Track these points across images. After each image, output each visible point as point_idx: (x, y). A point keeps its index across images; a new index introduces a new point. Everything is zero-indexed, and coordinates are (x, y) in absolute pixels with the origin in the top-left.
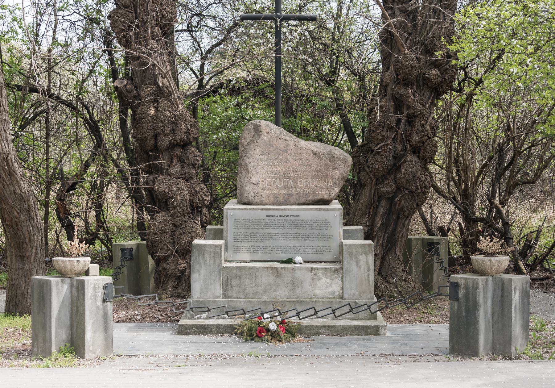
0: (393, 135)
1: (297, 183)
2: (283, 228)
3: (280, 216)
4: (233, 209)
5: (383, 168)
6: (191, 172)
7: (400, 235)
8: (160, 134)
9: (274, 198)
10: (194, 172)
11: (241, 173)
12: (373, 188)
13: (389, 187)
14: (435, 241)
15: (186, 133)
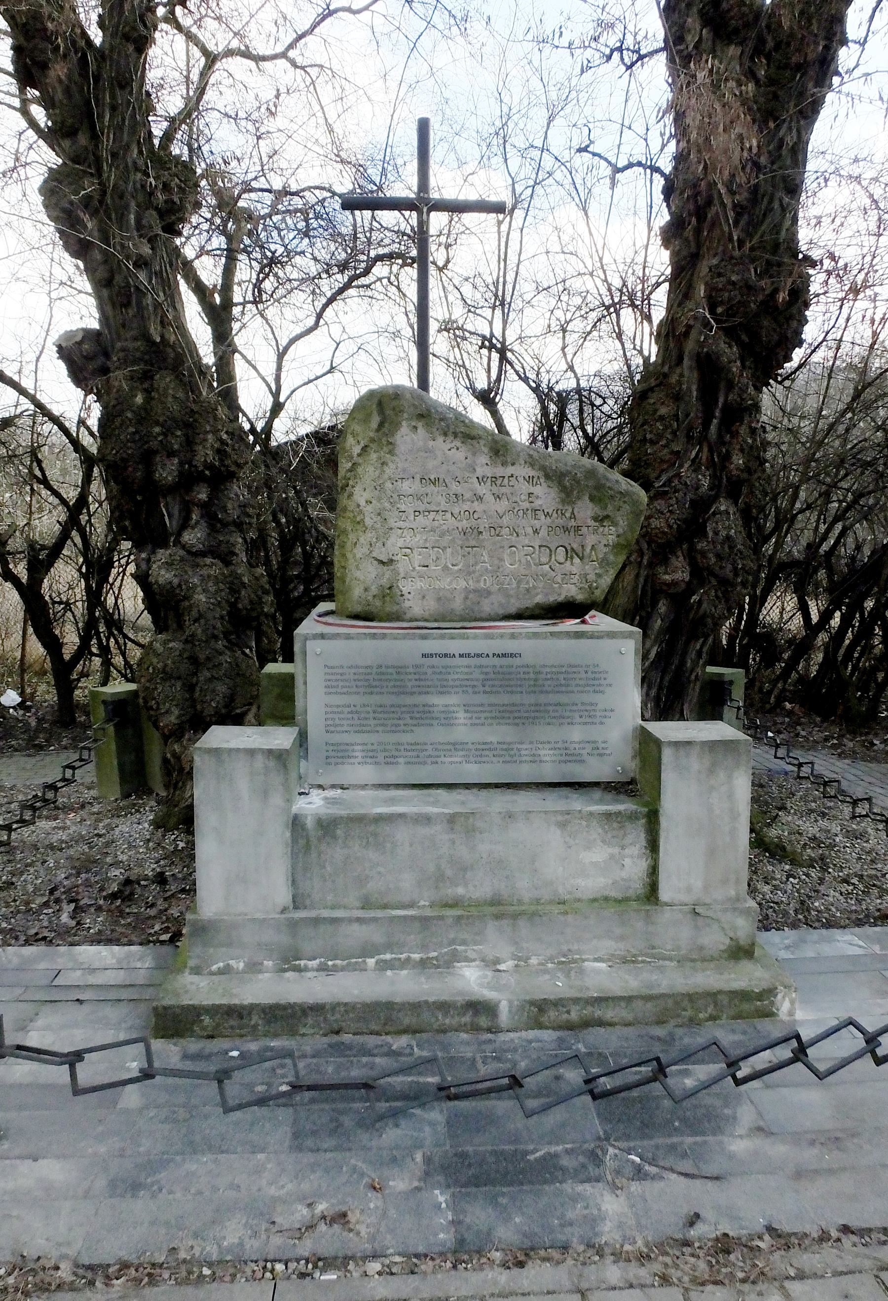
0: (694, 453)
1: (501, 560)
2: (470, 690)
3: (461, 656)
4: (323, 636)
5: (670, 527)
6: (232, 540)
7: (693, 677)
8: (156, 452)
9: (439, 599)
10: (240, 540)
11: (345, 532)
12: (644, 573)
13: (677, 572)
14: (727, 679)
15: (219, 451)
